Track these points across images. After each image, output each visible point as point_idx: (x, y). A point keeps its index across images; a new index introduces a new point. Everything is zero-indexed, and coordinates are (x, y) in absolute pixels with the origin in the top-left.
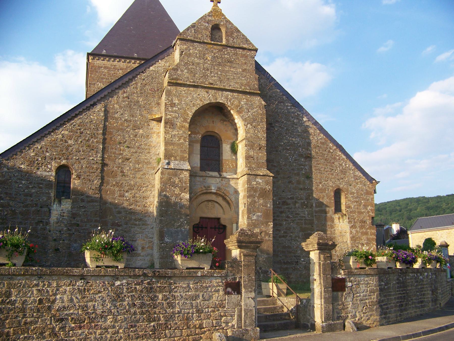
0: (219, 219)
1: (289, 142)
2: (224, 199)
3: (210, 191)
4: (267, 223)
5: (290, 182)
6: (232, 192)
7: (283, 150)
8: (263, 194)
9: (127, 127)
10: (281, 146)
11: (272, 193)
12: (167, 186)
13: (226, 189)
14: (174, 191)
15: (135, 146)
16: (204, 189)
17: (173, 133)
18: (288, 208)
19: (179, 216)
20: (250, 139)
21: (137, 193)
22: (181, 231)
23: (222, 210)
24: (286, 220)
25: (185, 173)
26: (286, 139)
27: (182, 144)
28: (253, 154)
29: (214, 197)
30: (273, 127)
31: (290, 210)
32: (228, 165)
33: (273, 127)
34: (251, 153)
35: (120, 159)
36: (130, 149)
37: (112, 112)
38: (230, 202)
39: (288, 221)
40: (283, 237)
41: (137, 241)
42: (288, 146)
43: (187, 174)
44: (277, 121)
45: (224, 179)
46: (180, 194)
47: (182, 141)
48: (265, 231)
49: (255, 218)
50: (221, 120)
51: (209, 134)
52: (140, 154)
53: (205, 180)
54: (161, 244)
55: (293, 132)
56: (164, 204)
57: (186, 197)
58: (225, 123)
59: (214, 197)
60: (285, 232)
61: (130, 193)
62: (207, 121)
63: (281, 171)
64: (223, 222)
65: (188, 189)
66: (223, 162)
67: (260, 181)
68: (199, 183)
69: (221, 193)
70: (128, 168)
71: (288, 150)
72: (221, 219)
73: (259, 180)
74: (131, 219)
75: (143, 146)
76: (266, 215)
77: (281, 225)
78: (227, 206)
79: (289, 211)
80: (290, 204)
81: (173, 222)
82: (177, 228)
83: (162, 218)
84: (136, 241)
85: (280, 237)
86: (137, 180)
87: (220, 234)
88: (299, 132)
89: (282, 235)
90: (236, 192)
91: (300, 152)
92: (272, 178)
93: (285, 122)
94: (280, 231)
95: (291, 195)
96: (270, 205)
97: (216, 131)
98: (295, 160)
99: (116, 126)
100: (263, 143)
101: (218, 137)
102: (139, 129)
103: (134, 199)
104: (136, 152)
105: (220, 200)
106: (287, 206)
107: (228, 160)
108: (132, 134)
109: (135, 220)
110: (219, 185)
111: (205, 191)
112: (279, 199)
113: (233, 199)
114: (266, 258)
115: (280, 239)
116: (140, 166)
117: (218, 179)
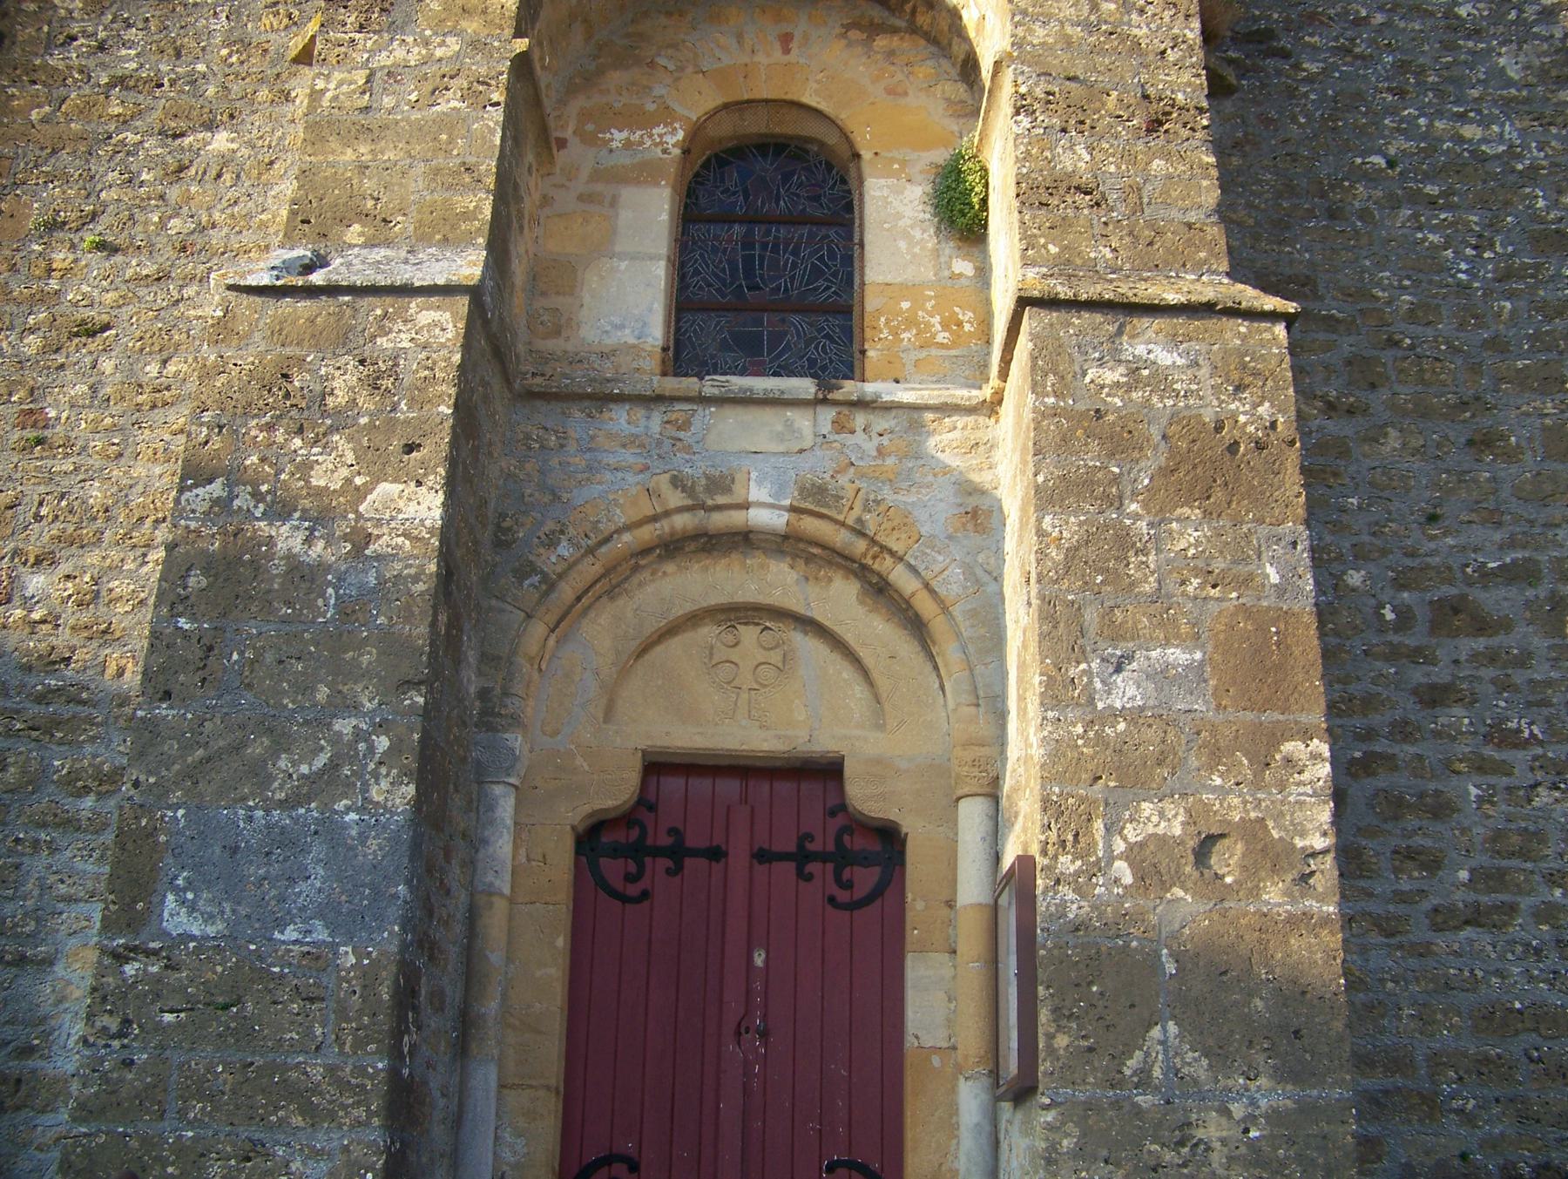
0: (829, 771)
1: (1432, 150)
2: (879, 590)
3: (736, 518)
4: (1262, 749)
5: (1483, 443)
6: (933, 511)
7: (1394, 204)
8: (1206, 468)
9: (124, 122)
10: (1371, 177)
11: (1292, 458)
12: (253, 429)
13: (886, 493)
14: (306, 467)
15: (160, 241)
16: (675, 499)
17: (383, 59)
18: (1492, 657)
19: (322, 693)
20: (1060, 61)
21: (116, 569)
22: (330, 828)
23: (859, 690)
24: (1481, 767)
25: (426, 317)
26: (1407, 129)
27: (450, 123)
28: (1095, 167)
29: (779, 582)
30: (1285, 55)
31: (1519, 677)
32: (911, 322)
33: (1285, 55)
34: (1075, 158)
35: (32, 331)
36: (119, 258)
37: (32, 41)
38: (925, 606)
39: (1505, 769)
40: (1475, 917)
41: (59, 969)
42: (1428, 178)
43: (440, 328)
44: (1312, 17)
45: (860, 419)
46: (361, 493)
47: (450, 103)
48: (1253, 831)
49: (1126, 691)
50: (848, 27)
51: (755, 125)
52: (190, 291)
53: (685, 426)
54: (120, 957)
55: (1459, 82)
56: (196, 581)
57: (411, 510)
58: (881, 42)
59: (779, 582)
60: (1485, 878)
61: (65, 568)
62: (740, 37)
63: (1387, 356)
64: (865, 795)
65: (436, 447)
66: (872, 302)
67: (1164, 357)
68: (628, 457)
69: (840, 538)
70: (82, 389)
71: (1432, 202)
72: (849, 770)
73: (1151, 346)
74: (35, 780)
75: (216, 238)
76: (1249, 665)
77: (1441, 809)
78: (906, 647)
79: (1503, 686)
80: (1505, 625)
81: (258, 747)
82: (287, 805)
83: (163, 710)
84: (49, 962)
85: (1443, 919)
86: (139, 470)
87: (854, 906)
88: (1510, 83)
89: (1459, 897)
90: (978, 514)
91: (1536, 218)
92: (1280, 330)
93: (1379, 18)
94: (1433, 864)
95: (1512, 544)
96: (1282, 569)
97: (806, 100)
98: (1505, 276)
99: (45, 120)
100: (1184, 82)
101: (832, 139)
102: (211, 126)
103: (85, 617)
104: (161, 278)
105: (838, 601)
106: (1480, 644)
107: (911, 290)
108: (152, 162)
109: (74, 785)
110: (819, 466)
111: (682, 522)
112: (1400, 584)
113: (952, 582)
114: (1275, 1117)
115: (1441, 942)
116: (171, 368)
117: (802, 420)
